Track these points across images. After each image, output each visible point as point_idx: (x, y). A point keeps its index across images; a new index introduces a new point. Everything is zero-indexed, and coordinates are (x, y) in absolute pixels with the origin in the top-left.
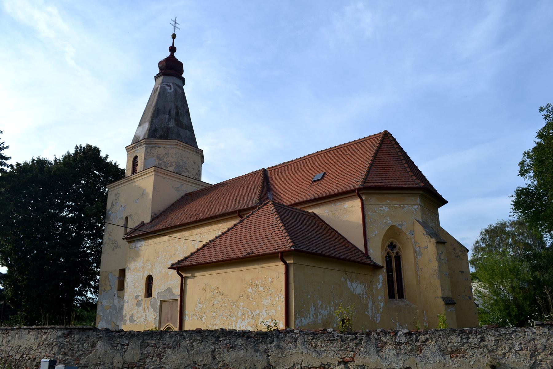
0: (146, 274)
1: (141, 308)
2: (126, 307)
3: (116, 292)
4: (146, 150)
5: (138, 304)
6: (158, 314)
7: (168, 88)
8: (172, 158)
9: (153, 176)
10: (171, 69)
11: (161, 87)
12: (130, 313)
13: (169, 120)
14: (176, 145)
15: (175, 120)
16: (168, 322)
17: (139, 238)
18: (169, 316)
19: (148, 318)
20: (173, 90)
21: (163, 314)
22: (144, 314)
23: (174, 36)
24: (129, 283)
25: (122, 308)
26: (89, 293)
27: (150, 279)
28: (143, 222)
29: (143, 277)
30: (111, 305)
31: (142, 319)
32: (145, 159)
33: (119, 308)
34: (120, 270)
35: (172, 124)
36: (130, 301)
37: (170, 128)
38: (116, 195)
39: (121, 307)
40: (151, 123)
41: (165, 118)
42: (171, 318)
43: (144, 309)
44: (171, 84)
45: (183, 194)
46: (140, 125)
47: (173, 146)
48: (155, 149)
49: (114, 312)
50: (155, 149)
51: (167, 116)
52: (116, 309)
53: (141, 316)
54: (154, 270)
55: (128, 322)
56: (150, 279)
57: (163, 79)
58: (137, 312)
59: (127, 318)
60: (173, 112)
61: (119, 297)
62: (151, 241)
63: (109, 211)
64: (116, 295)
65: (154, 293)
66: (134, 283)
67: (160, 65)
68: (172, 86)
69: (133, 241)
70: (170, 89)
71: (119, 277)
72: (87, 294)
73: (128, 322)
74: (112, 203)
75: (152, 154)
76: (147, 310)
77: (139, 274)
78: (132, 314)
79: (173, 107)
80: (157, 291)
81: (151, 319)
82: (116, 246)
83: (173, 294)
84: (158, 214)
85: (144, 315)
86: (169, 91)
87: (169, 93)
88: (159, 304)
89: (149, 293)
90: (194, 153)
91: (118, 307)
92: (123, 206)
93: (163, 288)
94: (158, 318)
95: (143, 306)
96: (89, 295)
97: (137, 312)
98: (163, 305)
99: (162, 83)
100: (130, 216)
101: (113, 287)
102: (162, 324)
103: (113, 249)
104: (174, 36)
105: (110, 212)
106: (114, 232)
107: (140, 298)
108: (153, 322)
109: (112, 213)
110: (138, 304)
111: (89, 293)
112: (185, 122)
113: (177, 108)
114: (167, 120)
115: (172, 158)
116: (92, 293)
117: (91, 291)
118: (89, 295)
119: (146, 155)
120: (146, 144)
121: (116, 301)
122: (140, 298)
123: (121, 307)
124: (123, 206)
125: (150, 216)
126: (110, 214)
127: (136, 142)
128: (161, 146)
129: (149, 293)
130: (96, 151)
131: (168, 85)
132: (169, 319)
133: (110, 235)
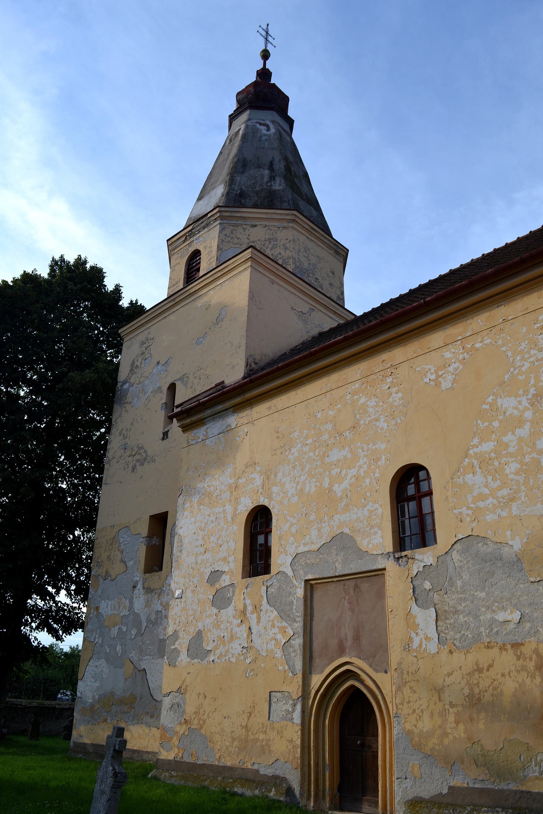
0: (246, 505)
1: (230, 611)
2: (175, 611)
3: (138, 577)
4: (220, 232)
5: (221, 600)
6: (299, 625)
7: (263, 129)
8: (286, 248)
9: (247, 273)
10: (263, 98)
11: (247, 127)
12: (192, 631)
13: (272, 178)
14: (293, 221)
15: (285, 177)
16: (341, 651)
17: (220, 407)
18: (348, 632)
19: (257, 642)
20: (273, 130)
21: (318, 626)
22: (244, 629)
23: (266, 55)
24: (186, 541)
25: (159, 618)
26: (63, 592)
27: (260, 521)
28: (223, 382)
29: (234, 516)
30: (125, 612)
31: (236, 647)
32: (219, 249)
33: (149, 621)
34: (154, 518)
35: (279, 185)
36: (189, 594)
37: (275, 191)
38: (143, 343)
39: (153, 617)
40: (231, 182)
41: (262, 177)
42: (357, 638)
43: (244, 612)
44: (268, 122)
45: (315, 332)
46: (200, 199)
47: (286, 224)
48: (244, 229)
49: (134, 632)
50: (244, 229)
51: (267, 172)
52: (137, 623)
53: (232, 638)
54: (275, 489)
55: (183, 658)
56: (260, 521)
57: (250, 115)
58: (217, 625)
59: (182, 644)
60: (280, 166)
61: (148, 590)
62: (260, 410)
63: (124, 383)
64: (140, 586)
65: (280, 560)
66: (207, 535)
67: (240, 97)
68: (271, 126)
69: (201, 423)
70: (268, 129)
71: (150, 536)
72: (58, 593)
73: (183, 658)
74: (133, 363)
75: (236, 241)
76: (253, 619)
77: (219, 509)
78: (199, 633)
79: (278, 157)
80: (292, 550)
81: (272, 645)
82: (141, 458)
83: (362, 554)
84: (263, 363)
85: (242, 632)
86: (264, 132)
87: (265, 135)
88: (300, 592)
89: (257, 559)
90: (331, 252)
91: (143, 618)
92: (162, 362)
93: (315, 539)
94: (298, 642)
95: (238, 601)
96: (63, 597)
97: (217, 625)
98: (318, 595)
99: (249, 120)
100: (181, 379)
101: (130, 564)
102: (317, 661)
103: (134, 469)
104: (266, 55)
105: (126, 386)
106: (139, 419)
107: (225, 580)
108: (279, 654)
109: (132, 385)
110: (221, 600)
111: (63, 592)
112: (305, 189)
113: (286, 159)
114: (266, 179)
115: (286, 248)
116: (69, 594)
117: (68, 590)
118: (63, 597)
119: (221, 242)
120: (222, 218)
121: (139, 602)
122: (225, 580)
123: (153, 617)
124: (162, 362)
125: (243, 364)
126: (128, 390)
127: (196, 224)
128: (258, 223)
129: (257, 559)
130: (97, 274)
131: (261, 124)
132: (349, 643)
133: (125, 437)
